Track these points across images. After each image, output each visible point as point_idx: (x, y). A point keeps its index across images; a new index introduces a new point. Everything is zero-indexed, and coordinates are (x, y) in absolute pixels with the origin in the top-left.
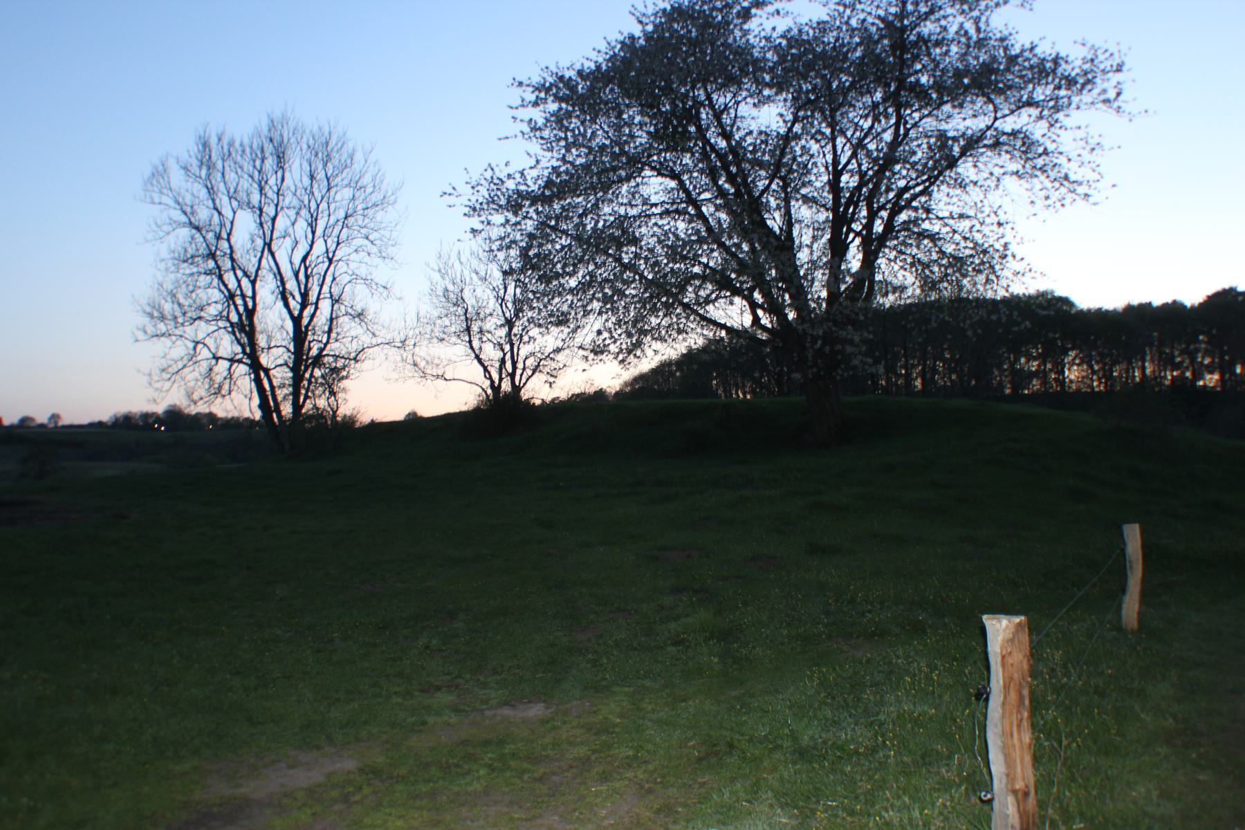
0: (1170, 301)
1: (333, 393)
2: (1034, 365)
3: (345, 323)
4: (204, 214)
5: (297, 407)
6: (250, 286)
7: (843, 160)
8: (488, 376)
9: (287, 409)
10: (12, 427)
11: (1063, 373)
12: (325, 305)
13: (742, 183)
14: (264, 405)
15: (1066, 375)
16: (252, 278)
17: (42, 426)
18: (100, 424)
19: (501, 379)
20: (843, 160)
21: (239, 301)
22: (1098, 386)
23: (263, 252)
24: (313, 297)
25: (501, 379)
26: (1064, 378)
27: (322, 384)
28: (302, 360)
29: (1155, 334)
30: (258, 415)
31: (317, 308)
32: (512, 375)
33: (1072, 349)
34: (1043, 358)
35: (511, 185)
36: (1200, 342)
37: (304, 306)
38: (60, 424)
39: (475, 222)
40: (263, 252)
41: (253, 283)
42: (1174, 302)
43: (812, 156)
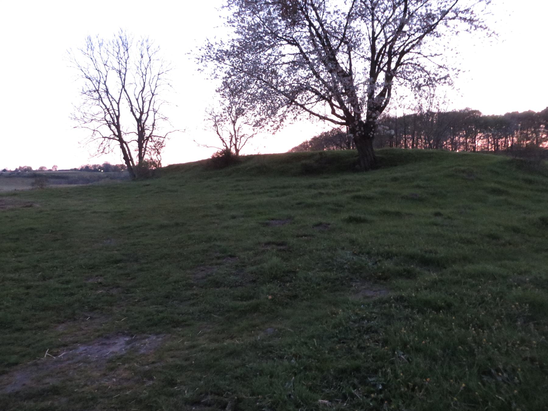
0: (527, 110)
1: (159, 153)
2: (462, 140)
3: (158, 123)
4: (93, 73)
5: (141, 156)
6: (117, 105)
7: (377, 32)
8: (225, 145)
9: (136, 160)
10: (34, 171)
11: (475, 143)
12: (151, 113)
13: (327, 45)
14: (126, 158)
15: (476, 144)
16: (117, 102)
17: (50, 170)
18: (75, 169)
19: (231, 147)
20: (377, 32)
21: (111, 112)
22: (492, 148)
23: (122, 90)
24: (145, 110)
25: (231, 147)
26: (475, 145)
27: (154, 149)
28: (142, 139)
29: (519, 125)
30: (123, 162)
31: (148, 115)
32: (235, 145)
33: (480, 132)
34: (466, 137)
35: (217, 47)
36: (541, 128)
37: (142, 113)
38: (58, 169)
39: (201, 66)
40: (122, 90)
41: (118, 104)
42: (529, 111)
43: (363, 35)
